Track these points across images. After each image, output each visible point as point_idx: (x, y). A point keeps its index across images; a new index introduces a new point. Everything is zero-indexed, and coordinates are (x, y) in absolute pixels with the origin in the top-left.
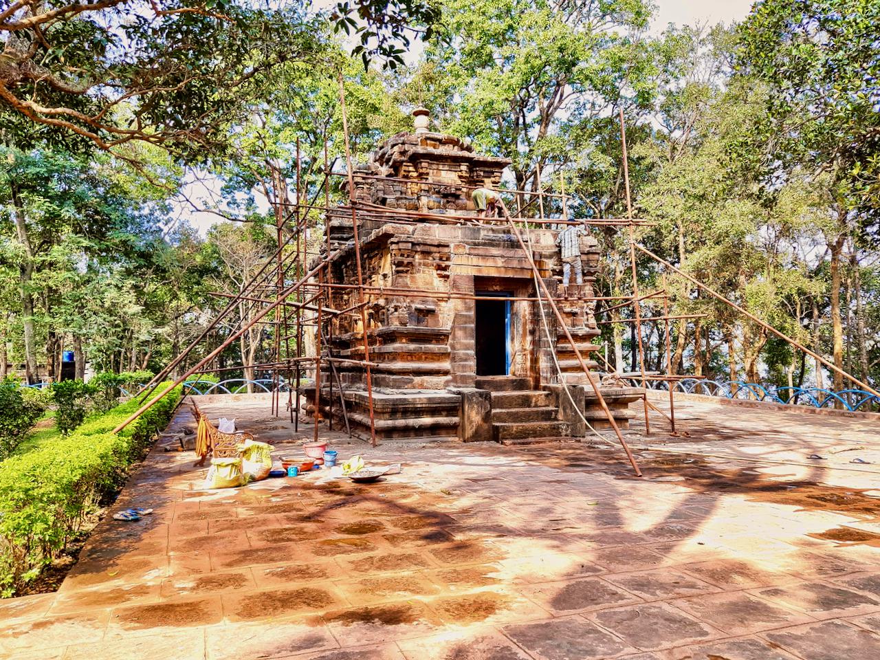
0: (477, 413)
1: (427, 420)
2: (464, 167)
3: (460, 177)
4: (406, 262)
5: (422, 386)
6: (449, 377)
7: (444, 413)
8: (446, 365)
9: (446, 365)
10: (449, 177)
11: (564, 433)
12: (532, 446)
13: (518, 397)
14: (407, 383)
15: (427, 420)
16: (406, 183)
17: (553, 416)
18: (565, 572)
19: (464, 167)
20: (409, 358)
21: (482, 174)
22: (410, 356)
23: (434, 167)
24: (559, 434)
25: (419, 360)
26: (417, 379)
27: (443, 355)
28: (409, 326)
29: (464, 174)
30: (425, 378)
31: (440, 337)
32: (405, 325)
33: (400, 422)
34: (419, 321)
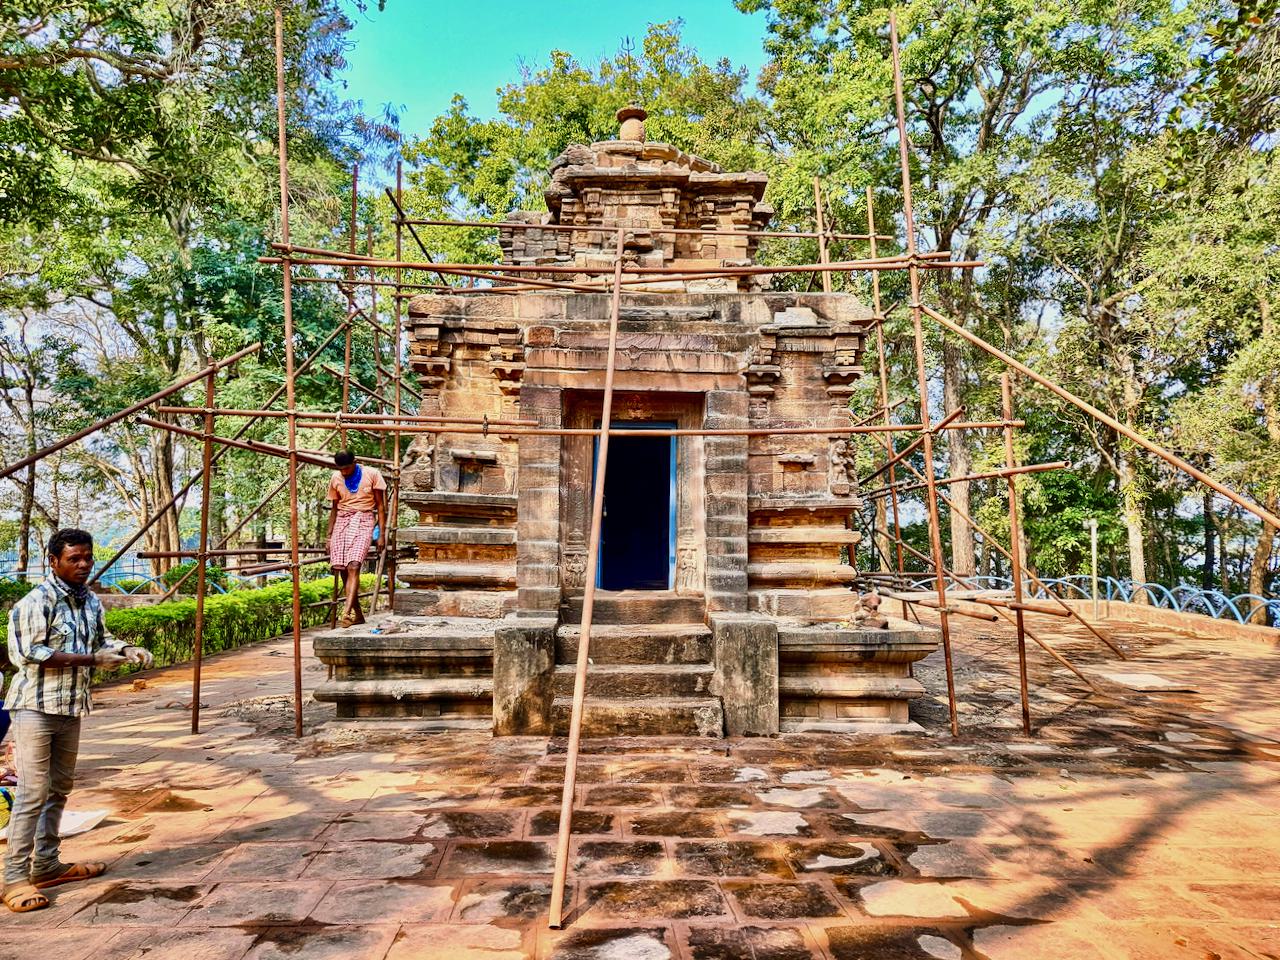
0: (521, 675)
1: (425, 687)
2: (669, 196)
3: (663, 215)
4: (429, 365)
5: (455, 610)
6: (514, 594)
7: (468, 671)
8: (505, 571)
9: (505, 571)
10: (637, 216)
11: (704, 729)
12: (832, 722)
13: (635, 640)
14: (423, 604)
15: (425, 687)
16: (571, 231)
17: (699, 687)
18: (1129, 882)
19: (669, 196)
20: (440, 554)
21: (711, 206)
22: (439, 548)
23: (613, 200)
24: (693, 730)
25: (462, 557)
26: (446, 597)
27: (508, 549)
28: (439, 491)
29: (670, 209)
30: (465, 595)
31: (502, 513)
32: (429, 488)
33: (367, 687)
34: (462, 480)
